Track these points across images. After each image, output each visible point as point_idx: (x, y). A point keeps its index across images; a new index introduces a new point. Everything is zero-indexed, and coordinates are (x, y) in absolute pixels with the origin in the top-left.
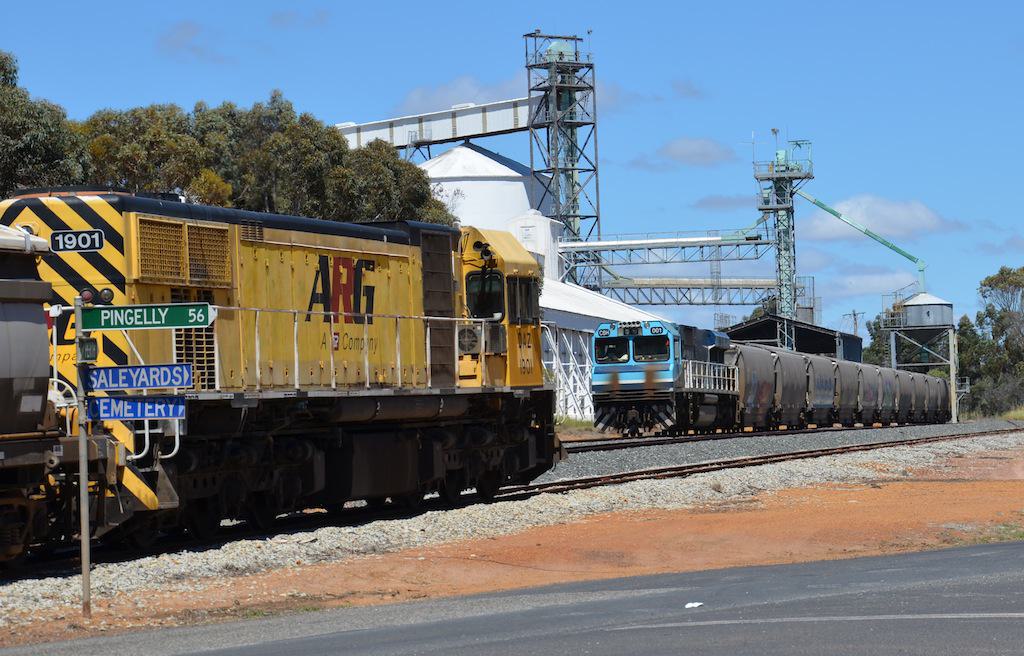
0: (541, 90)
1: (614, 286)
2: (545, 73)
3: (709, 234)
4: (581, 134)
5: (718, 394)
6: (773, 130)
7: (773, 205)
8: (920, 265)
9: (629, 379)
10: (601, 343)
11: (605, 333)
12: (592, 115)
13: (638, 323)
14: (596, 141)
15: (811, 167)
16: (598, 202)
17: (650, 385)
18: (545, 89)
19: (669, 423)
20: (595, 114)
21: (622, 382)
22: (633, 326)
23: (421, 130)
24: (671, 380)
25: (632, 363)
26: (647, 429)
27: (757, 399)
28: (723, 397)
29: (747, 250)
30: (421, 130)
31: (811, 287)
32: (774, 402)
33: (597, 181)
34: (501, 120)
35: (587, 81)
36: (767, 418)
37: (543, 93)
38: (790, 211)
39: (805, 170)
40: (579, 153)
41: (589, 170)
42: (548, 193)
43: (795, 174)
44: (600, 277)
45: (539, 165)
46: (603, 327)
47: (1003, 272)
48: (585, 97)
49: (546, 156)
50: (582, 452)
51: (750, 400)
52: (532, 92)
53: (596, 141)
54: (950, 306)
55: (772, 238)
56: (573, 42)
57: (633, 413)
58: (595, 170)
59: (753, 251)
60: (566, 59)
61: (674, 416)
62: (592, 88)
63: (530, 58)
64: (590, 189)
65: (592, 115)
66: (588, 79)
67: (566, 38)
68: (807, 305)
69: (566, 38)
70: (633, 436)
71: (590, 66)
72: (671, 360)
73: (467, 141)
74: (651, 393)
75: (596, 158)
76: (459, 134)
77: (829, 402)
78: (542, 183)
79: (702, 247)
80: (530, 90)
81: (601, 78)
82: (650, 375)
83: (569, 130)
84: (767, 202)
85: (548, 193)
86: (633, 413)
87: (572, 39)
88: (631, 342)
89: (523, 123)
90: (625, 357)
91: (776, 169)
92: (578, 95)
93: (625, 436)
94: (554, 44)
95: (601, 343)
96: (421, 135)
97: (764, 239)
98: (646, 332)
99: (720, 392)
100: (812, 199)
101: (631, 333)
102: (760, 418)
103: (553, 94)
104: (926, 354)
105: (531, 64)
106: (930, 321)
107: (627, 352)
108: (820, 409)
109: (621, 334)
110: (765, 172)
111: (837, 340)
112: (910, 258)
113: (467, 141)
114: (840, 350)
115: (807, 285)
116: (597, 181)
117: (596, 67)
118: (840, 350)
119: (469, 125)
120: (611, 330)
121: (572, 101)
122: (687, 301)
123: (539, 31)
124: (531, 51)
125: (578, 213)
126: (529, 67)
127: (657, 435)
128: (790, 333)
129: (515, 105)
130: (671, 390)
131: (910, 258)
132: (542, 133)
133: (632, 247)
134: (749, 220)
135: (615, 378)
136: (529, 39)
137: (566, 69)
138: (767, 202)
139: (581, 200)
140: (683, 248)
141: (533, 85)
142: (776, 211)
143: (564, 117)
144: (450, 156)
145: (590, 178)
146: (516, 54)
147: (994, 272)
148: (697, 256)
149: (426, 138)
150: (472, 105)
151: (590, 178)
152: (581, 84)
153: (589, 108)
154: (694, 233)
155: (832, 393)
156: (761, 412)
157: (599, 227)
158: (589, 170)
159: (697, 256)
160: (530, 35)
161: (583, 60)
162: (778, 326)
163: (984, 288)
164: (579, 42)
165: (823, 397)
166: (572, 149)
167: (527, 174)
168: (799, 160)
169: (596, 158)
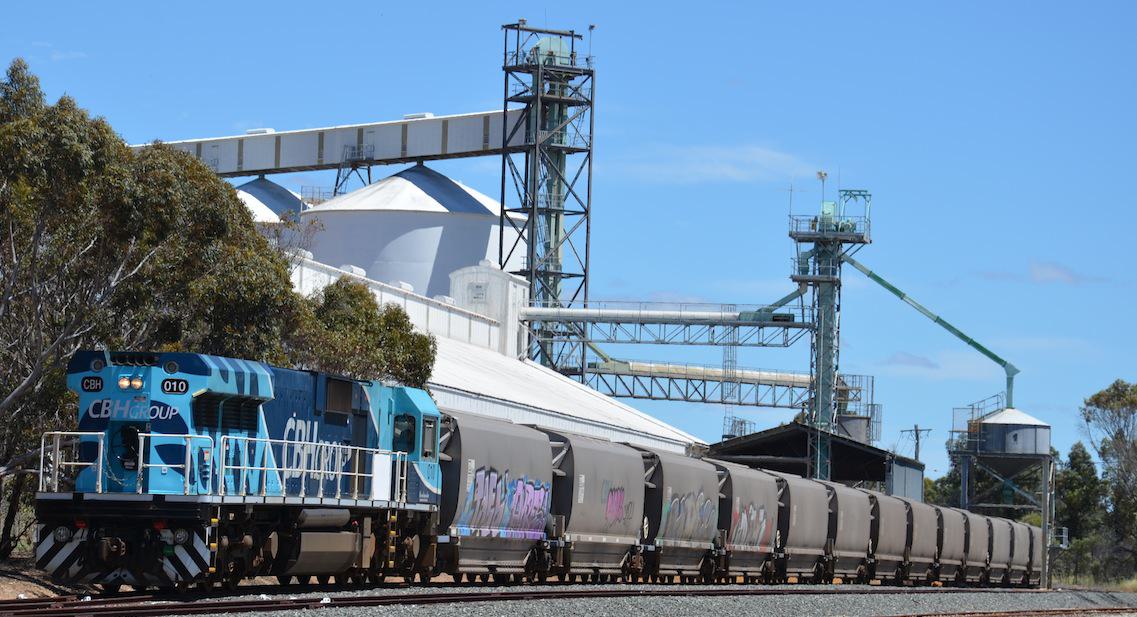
29: (772, 333)
47: (1116, 386)
48: (580, 115)
52: (509, 103)
58: (586, 212)
60: (558, 62)
80: (506, 101)
92: (570, 111)
115: (864, 387)
117: (597, 75)
123: (523, 22)
124: (512, 48)
137: (560, 76)
141: (511, 94)
145: (581, 222)
147: (1103, 385)
151: (581, 222)
160: (511, 27)
161: (581, 64)
163: (1090, 408)
164: (576, 39)
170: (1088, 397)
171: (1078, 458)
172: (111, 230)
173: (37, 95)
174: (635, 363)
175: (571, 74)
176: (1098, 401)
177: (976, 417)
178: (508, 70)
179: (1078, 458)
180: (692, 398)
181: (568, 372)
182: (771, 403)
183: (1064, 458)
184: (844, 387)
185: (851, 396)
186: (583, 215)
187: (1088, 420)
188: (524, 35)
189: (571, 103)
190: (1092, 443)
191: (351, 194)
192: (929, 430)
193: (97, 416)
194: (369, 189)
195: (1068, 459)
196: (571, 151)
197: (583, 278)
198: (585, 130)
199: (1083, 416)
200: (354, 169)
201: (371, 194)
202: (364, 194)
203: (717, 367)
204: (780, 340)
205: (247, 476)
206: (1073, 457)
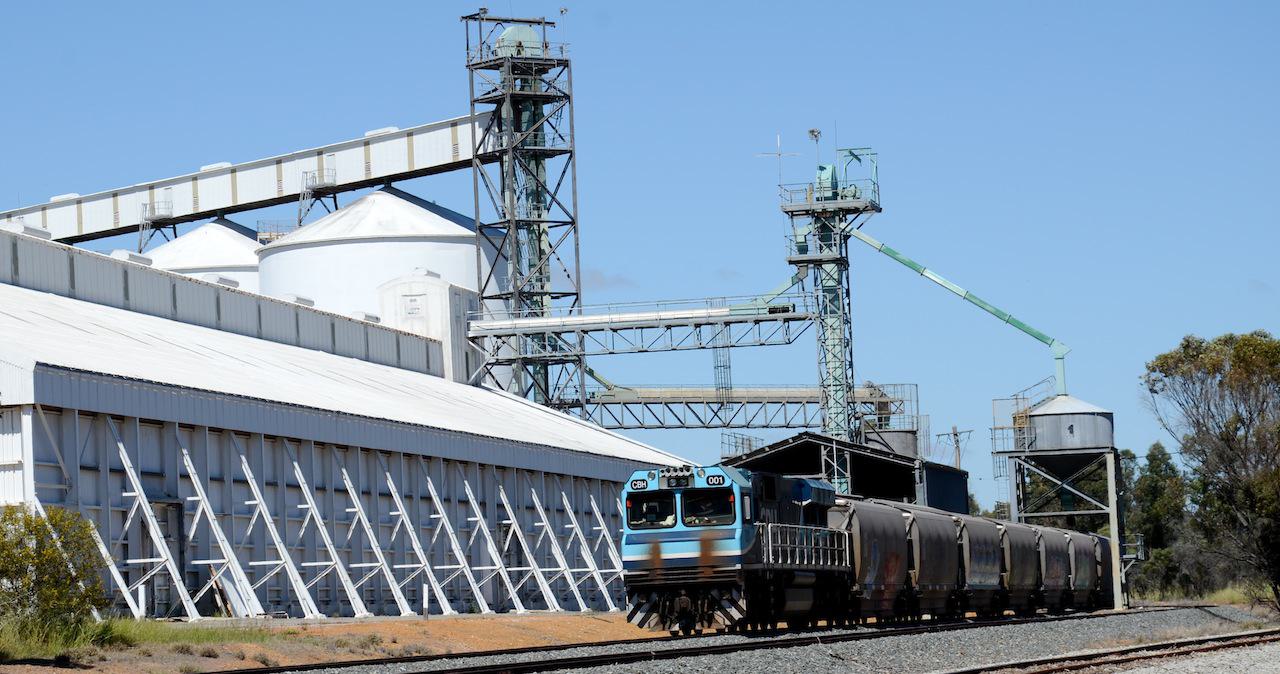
0: (490, 101)
1: (605, 399)
2: (495, 77)
3: (710, 303)
4: (552, 168)
5: (816, 572)
6: (812, 132)
7: (813, 254)
8: (1058, 349)
9: (673, 552)
10: (635, 499)
11: (640, 485)
12: (568, 139)
13: (688, 468)
14: (574, 179)
15: (876, 191)
16: (490, 241)
17: (707, 560)
18: (499, 102)
19: (736, 615)
20: (572, 137)
21: (665, 556)
22: (681, 474)
23: (321, 169)
24: (738, 552)
25: (680, 527)
26: (706, 624)
27: (880, 579)
28: (822, 575)
29: (772, 330)
30: (321, 169)
31: (914, 399)
32: (1068, 583)
33: (577, 239)
34: (434, 149)
35: (558, 86)
36: (950, 603)
37: (493, 107)
38: (842, 263)
39: (867, 197)
40: (549, 199)
41: (565, 223)
42: (500, 257)
43: (849, 203)
44: (582, 385)
45: (489, 216)
46: (639, 475)
47: (1187, 345)
48: (557, 113)
49: (499, 203)
50: (798, 645)
51: (869, 579)
52: (476, 105)
53: (574, 179)
54: (1109, 416)
55: (813, 310)
56: (541, 27)
57: (683, 600)
58: (573, 223)
59: (781, 332)
60: (526, 53)
61: (742, 603)
62: (567, 97)
63: (472, 54)
64: (566, 251)
65: (568, 139)
66: (562, 84)
67: (530, 22)
68: (908, 428)
69: (530, 22)
70: (687, 635)
71: (565, 64)
72: (738, 525)
73: (387, 183)
74: (709, 572)
75: (575, 205)
76: (376, 174)
77: (994, 581)
78: (493, 245)
79: (698, 326)
80: (474, 102)
81: (581, 82)
82: (706, 545)
83: (533, 163)
84: (803, 249)
85: (500, 257)
86: (683, 600)
87: (539, 23)
88: (678, 496)
89: (466, 154)
90: (670, 520)
91: (818, 195)
92: (547, 109)
93: (675, 636)
94: (510, 28)
95: (635, 499)
96: (321, 176)
97: (800, 312)
98: (700, 483)
99: (818, 567)
100: (878, 244)
101: (678, 485)
102: (886, 605)
103: (506, 111)
104: (1070, 496)
105: (474, 62)
106: (1075, 441)
107: (672, 511)
108: (979, 591)
109: (665, 487)
110: (800, 202)
111: (917, 473)
112: (1040, 338)
113: (387, 183)
114: (921, 490)
115: (907, 397)
116: (577, 239)
117: (573, 65)
118: (921, 490)
119: (389, 159)
120: (649, 481)
121: (536, 116)
122: (720, 423)
123: (484, 11)
124: (475, 42)
125: (548, 288)
126: (472, 67)
127: (720, 632)
128: (842, 464)
129: (454, 124)
130: (738, 566)
131: (1040, 338)
132: (493, 169)
133: (585, 328)
134: (778, 283)
135: (656, 551)
136: (471, 22)
137: (525, 68)
138: (803, 249)
139: (554, 267)
140: (669, 327)
141: (478, 95)
142: (818, 263)
143: (523, 142)
144: (360, 208)
145: (567, 233)
146: (452, 48)
147: (1172, 345)
148: (692, 341)
149: (328, 181)
150: (394, 130)
151: (567, 233)
152: (552, 92)
153: (564, 129)
154: (683, 303)
155: (997, 569)
156: (887, 596)
157: (479, 279)
158: (565, 223)
159: (692, 341)
160: (472, 17)
161: (554, 54)
162: (824, 452)
163: (1154, 376)
164: (548, 27)
165: (983, 574)
166: (538, 195)
167: (484, 232)
168: (858, 183)
169: (575, 205)
170: (1151, 358)
171: (1157, 457)
172: (1122, 480)
173: (472, 293)
174: (643, 390)
175: (543, 67)
176: (1166, 366)
177: (1021, 408)
178: (472, 67)
179: (1157, 457)
180: (713, 423)
181: (562, 406)
182: (783, 423)
183: (1143, 462)
184: (883, 400)
185: (893, 408)
186: (569, 226)
187: (1152, 391)
188: (487, 26)
189: (549, 99)
190: (1160, 419)
191: (307, 227)
192: (970, 432)
193: (651, 504)
194: (336, 215)
195: (1147, 462)
196: (552, 154)
197: (575, 297)
198: (564, 129)
199: (1146, 386)
200: (318, 198)
201: (333, 222)
202: (325, 223)
203: (707, 386)
204: (779, 337)
205: (277, 565)
206: (1151, 458)
